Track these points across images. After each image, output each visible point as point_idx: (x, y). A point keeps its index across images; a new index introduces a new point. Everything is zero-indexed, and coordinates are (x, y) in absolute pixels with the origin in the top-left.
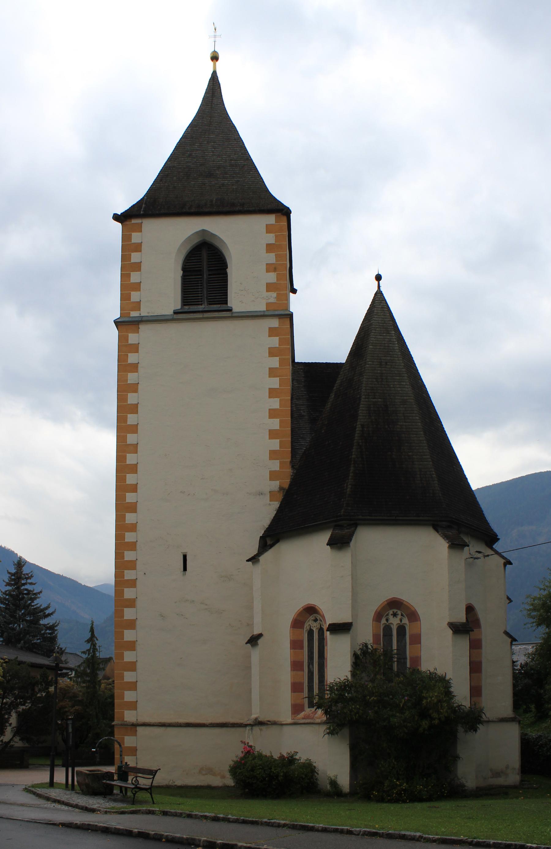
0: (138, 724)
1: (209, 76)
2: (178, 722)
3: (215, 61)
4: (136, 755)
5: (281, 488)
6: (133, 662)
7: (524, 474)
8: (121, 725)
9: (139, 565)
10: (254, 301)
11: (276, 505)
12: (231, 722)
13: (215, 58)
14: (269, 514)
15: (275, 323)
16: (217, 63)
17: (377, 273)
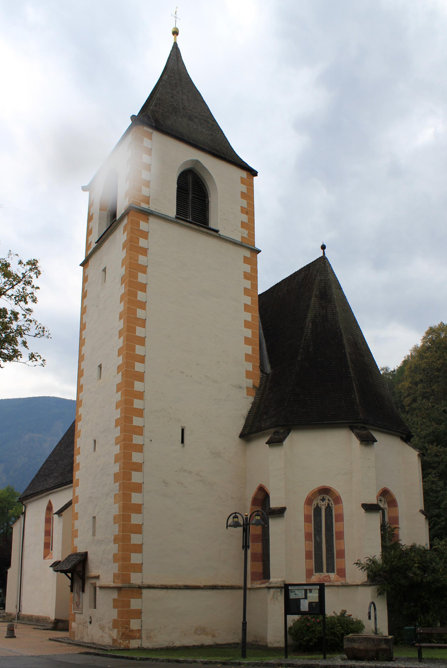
0: (143, 586)
1: (172, 45)
2: (177, 585)
3: (175, 35)
4: (140, 618)
5: (254, 387)
6: (138, 525)
7: (37, 396)
8: (129, 587)
9: (146, 432)
10: (233, 231)
11: (251, 399)
12: (220, 585)
13: (175, 33)
14: (246, 406)
15: (248, 254)
16: (178, 37)
17: (322, 244)
